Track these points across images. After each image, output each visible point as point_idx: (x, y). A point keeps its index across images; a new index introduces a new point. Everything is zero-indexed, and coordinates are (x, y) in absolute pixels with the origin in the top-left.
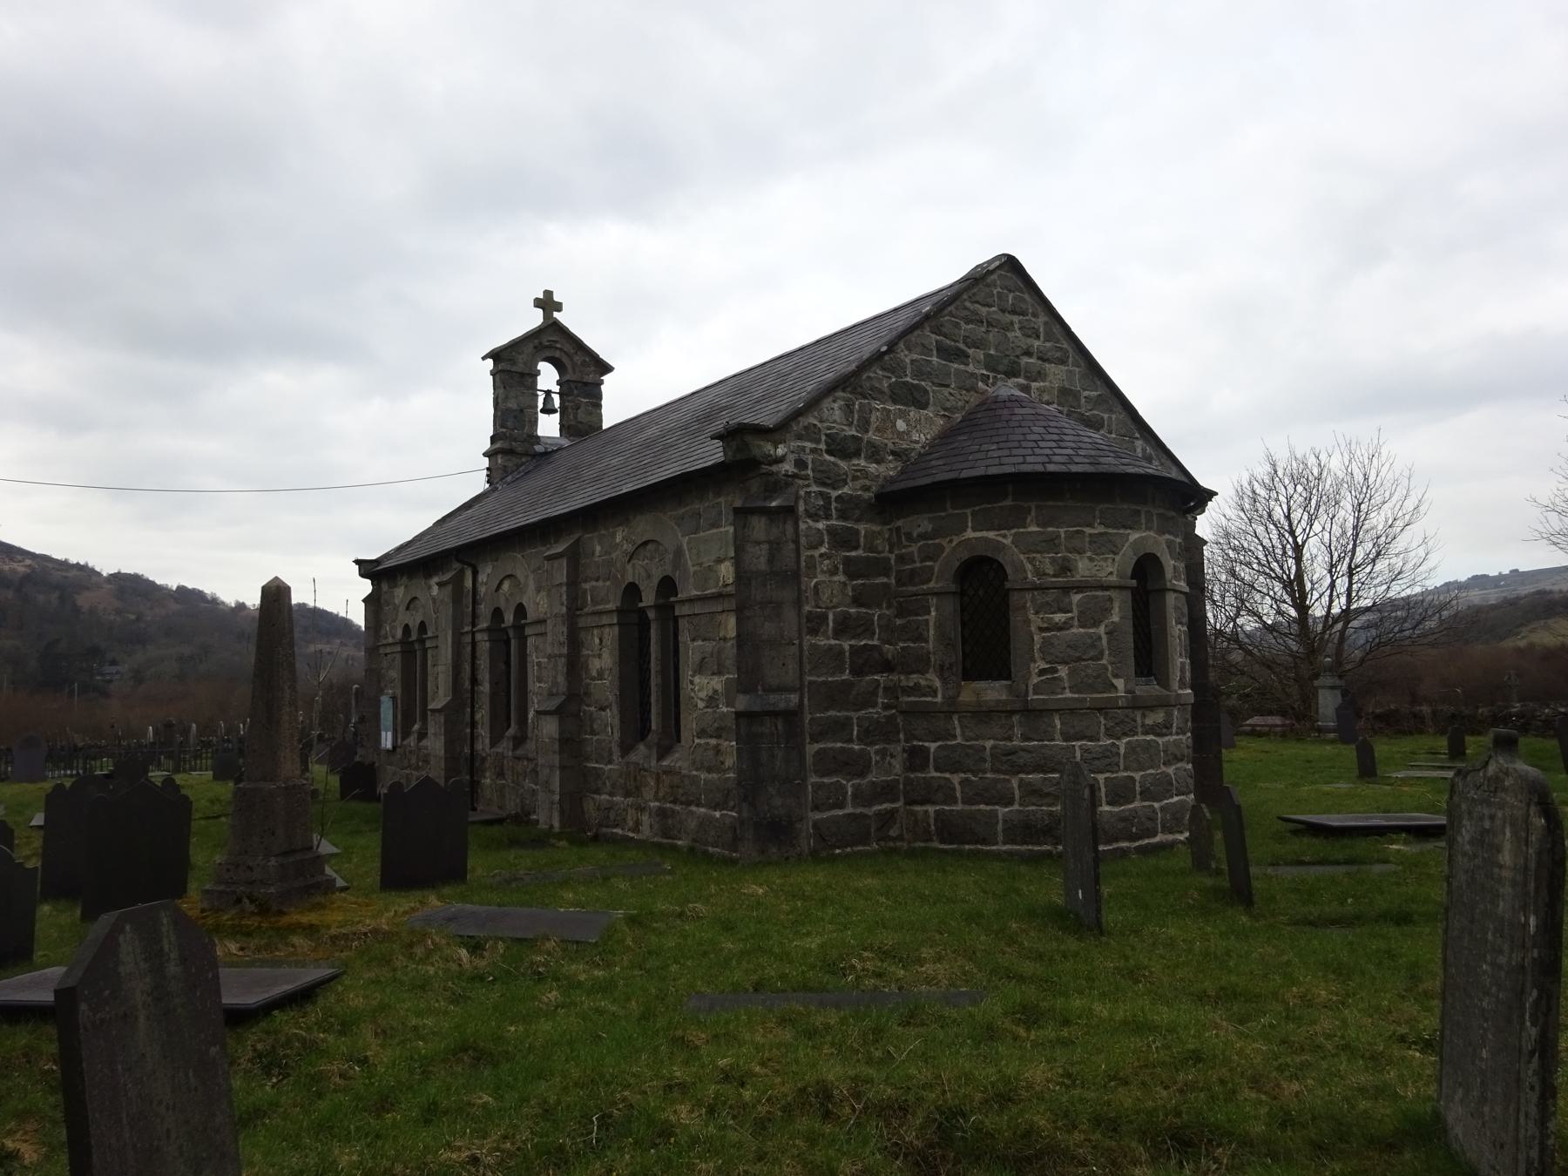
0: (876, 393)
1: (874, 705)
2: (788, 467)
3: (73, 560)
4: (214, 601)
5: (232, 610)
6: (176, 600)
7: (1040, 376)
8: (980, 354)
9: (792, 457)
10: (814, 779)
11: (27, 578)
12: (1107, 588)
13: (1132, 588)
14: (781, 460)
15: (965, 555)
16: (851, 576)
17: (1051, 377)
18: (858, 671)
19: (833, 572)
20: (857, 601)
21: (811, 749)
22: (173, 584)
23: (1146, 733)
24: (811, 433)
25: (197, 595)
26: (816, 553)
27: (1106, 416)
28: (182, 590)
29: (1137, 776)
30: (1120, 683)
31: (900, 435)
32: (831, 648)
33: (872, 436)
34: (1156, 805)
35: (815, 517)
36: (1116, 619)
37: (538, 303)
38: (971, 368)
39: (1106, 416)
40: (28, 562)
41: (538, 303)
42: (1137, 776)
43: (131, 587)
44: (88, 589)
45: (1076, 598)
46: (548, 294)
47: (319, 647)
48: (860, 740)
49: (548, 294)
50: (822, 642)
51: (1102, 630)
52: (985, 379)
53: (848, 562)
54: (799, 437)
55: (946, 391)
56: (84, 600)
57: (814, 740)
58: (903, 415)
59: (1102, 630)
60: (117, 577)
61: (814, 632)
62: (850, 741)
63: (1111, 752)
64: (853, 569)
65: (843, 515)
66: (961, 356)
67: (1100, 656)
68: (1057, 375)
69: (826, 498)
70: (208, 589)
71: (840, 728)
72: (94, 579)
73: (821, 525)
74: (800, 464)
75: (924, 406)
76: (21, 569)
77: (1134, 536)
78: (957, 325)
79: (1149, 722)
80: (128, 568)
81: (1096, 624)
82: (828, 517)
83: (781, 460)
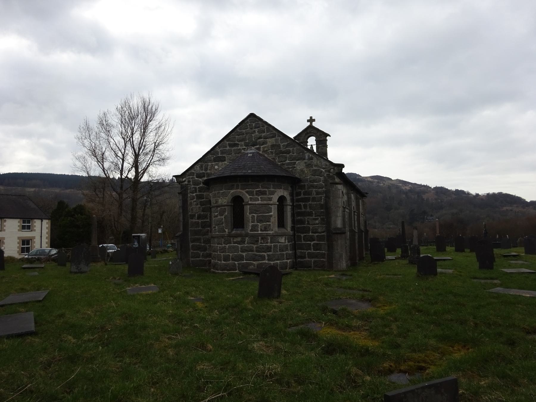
0: (210, 161)
1: (208, 235)
2: (186, 183)
3: (423, 184)
4: (469, 194)
5: (474, 196)
6: (455, 195)
7: (264, 143)
8: (243, 143)
9: (187, 180)
10: (192, 251)
11: (411, 191)
12: (224, 206)
13: (231, 205)
14: (185, 181)
15: (243, 197)
16: (201, 205)
17: (268, 143)
18: (203, 227)
19: (197, 204)
20: (203, 211)
21: (191, 244)
22: (453, 189)
23: (234, 243)
24: (192, 174)
25: (462, 192)
26: (192, 201)
27: (291, 149)
28: (457, 191)
29: (231, 255)
30: (227, 230)
31: (216, 170)
32: (196, 222)
33: (208, 171)
34: (236, 263)
35: (193, 193)
36: (226, 214)
37: (308, 121)
38: (239, 147)
39: (291, 149)
40: (410, 186)
41: (308, 121)
42: (231, 255)
43: (441, 191)
44: (427, 193)
45: (219, 209)
46: (311, 117)
47: (508, 208)
48: (204, 243)
49: (311, 117)
50: (194, 221)
51: (223, 217)
52: (244, 149)
53: (201, 202)
54: (189, 176)
55: (230, 156)
56: (425, 197)
57: (192, 242)
58: (216, 165)
59: (223, 217)
60: (436, 188)
61: (192, 218)
62: (201, 243)
63: (225, 247)
64: (202, 204)
65: (200, 191)
66: (237, 145)
67: (222, 224)
68: (271, 141)
69: (195, 188)
70: (465, 190)
71: (198, 240)
72: (394, 191)
73: (194, 195)
74: (189, 182)
75: (225, 161)
76: (408, 188)
77: (232, 191)
78: (235, 137)
79: (235, 240)
80: (439, 185)
81: (222, 215)
82: (196, 192)
83: (185, 181)
